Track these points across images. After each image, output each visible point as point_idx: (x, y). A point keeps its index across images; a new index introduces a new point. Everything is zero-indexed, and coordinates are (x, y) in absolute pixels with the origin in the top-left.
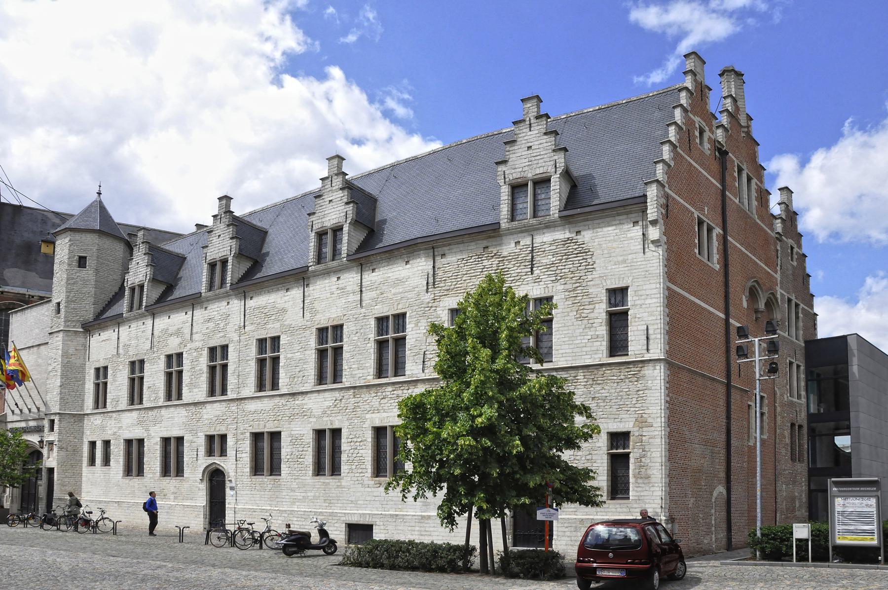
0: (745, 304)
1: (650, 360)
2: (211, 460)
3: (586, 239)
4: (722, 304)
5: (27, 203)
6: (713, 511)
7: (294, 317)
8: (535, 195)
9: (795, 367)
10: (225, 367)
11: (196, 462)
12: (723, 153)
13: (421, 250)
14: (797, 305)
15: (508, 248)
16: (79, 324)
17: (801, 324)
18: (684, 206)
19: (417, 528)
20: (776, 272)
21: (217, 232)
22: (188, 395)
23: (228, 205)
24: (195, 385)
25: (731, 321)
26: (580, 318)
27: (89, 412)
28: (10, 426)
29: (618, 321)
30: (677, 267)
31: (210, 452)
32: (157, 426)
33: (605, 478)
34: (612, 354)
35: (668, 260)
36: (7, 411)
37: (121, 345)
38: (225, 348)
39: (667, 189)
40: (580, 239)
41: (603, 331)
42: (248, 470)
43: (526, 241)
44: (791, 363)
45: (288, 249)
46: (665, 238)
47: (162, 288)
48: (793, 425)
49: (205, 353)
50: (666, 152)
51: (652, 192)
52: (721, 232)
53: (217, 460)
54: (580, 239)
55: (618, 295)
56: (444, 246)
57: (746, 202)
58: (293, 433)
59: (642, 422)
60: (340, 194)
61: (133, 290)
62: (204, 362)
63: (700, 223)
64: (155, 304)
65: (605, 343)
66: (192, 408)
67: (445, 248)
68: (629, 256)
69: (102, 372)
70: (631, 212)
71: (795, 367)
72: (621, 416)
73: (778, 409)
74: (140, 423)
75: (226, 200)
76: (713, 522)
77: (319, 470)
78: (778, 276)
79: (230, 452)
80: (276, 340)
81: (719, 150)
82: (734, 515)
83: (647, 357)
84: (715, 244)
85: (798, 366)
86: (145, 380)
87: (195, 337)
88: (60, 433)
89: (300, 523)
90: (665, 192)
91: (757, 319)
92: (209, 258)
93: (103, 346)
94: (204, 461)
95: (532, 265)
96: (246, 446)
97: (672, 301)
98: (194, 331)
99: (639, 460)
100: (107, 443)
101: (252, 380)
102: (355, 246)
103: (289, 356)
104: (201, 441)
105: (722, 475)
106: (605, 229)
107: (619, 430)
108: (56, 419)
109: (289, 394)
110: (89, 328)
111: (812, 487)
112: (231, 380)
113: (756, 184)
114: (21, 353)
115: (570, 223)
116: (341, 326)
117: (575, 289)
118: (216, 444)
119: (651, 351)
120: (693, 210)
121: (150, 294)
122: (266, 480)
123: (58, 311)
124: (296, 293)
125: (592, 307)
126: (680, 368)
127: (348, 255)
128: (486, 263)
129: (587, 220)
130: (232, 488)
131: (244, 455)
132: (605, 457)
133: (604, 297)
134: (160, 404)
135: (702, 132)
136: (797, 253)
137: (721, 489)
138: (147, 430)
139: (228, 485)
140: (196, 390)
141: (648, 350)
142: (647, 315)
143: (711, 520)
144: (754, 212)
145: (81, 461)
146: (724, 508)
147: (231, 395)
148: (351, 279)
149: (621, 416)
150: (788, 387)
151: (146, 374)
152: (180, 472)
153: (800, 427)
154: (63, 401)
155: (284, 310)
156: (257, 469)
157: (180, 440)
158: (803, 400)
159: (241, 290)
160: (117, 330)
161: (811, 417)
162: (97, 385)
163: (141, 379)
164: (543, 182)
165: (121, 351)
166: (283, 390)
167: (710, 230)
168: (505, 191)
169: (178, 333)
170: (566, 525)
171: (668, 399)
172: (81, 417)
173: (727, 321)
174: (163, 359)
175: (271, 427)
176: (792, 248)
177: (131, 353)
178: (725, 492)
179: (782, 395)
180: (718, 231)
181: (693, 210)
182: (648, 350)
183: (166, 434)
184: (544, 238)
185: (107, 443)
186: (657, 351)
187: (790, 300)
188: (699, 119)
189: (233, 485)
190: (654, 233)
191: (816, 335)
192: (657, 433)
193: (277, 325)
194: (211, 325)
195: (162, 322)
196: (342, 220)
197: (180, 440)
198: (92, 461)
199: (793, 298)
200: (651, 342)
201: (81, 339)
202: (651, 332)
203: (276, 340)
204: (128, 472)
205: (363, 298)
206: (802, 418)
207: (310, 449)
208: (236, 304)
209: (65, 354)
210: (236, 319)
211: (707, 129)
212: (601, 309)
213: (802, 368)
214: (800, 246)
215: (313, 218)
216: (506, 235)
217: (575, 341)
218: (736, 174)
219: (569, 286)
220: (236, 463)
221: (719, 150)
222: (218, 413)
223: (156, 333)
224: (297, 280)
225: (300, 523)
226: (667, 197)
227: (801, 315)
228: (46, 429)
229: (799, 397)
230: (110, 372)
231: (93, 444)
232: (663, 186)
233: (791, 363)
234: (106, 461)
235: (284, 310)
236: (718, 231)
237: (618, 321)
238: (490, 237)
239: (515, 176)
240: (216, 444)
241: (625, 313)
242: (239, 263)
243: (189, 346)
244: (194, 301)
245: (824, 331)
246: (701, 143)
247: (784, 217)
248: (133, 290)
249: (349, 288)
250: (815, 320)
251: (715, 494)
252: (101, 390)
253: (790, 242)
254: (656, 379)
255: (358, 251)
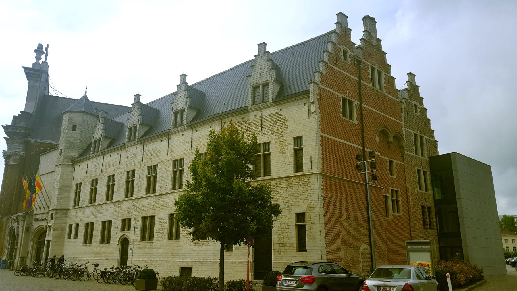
0: (377, 140)
1: (313, 174)
2: (123, 233)
3: (284, 113)
4: (360, 141)
5: (60, 95)
6: (360, 260)
7: (164, 155)
8: (263, 91)
9: (422, 173)
10: (133, 181)
11: (116, 235)
12: (359, 62)
13: (216, 120)
14: (421, 138)
15: (251, 117)
16: (70, 161)
17: (425, 148)
18: (333, 93)
19: (211, 269)
20: (401, 120)
21: (133, 113)
22: (116, 198)
23: (139, 99)
24: (119, 194)
25: (366, 149)
26: (282, 153)
27: (71, 208)
28: (34, 217)
29: (298, 153)
30: (327, 124)
31: (123, 229)
32: (97, 216)
33: (295, 239)
34: (296, 172)
35: (321, 121)
36: (34, 209)
37: (88, 171)
38: (134, 171)
39: (321, 86)
40: (282, 112)
41: (292, 159)
42: (139, 238)
43: (259, 114)
44: (419, 171)
45: (168, 120)
46: (319, 111)
47: (109, 141)
48: (423, 207)
49: (125, 174)
50: (321, 67)
51: (312, 87)
52: (359, 103)
53: (126, 233)
54: (282, 112)
55: (298, 140)
56: (225, 118)
57: (377, 85)
58: (160, 216)
59: (310, 207)
60: (184, 93)
61: (130, 129)
62: (124, 178)
63: (344, 100)
64: (106, 148)
65: (292, 165)
66: (117, 204)
67: (226, 119)
68: (302, 121)
69: (79, 186)
70: (303, 98)
71: (422, 173)
72: (301, 204)
73: (411, 198)
74: (93, 213)
75: (138, 96)
76: (361, 266)
77: (170, 238)
78: (403, 123)
79: (132, 228)
80: (156, 166)
81: (357, 60)
82: (41, 213)
83: (312, 172)
84: (355, 110)
85: (425, 173)
86: (97, 190)
87: (121, 166)
88: (55, 221)
89: (160, 268)
90: (319, 87)
91: (389, 147)
92: (129, 125)
93: (83, 172)
94: (120, 234)
95: (262, 126)
96: (139, 225)
97: (324, 142)
98: (121, 163)
99: (310, 228)
100: (77, 225)
101: (144, 188)
102: (191, 118)
103: (161, 175)
104: (120, 223)
105: (366, 238)
106: (292, 107)
107: (300, 212)
108: (54, 212)
109: (160, 195)
110: (74, 163)
111: (441, 245)
112: (136, 188)
113: (385, 75)
114: (42, 177)
115: (277, 105)
116: (183, 159)
117: (279, 138)
118: (126, 224)
119: (313, 169)
120: (338, 94)
121: (140, 132)
122: (146, 243)
123: (61, 154)
124: (165, 142)
125: (287, 147)
126: (330, 177)
127: (186, 123)
128: (243, 126)
129: (285, 103)
130: (131, 249)
131: (138, 230)
132: (295, 227)
133: (292, 141)
134: (103, 202)
135: (345, 53)
136: (420, 108)
137: (365, 246)
138: (96, 217)
139: (130, 247)
140: (119, 195)
141: (311, 168)
142: (311, 150)
143: (359, 265)
144: (384, 90)
145: (64, 236)
146: (369, 257)
147: (135, 196)
148: (188, 134)
149: (301, 204)
150: (418, 184)
151: (98, 186)
152: (109, 241)
153: (429, 208)
154: (59, 202)
155: (160, 151)
156: (143, 238)
157: (110, 222)
158: (430, 192)
159: (142, 142)
160: (120, 154)
161: (436, 201)
162: (76, 193)
163: (96, 189)
164: (266, 85)
165: (88, 174)
166: (157, 193)
167: (351, 103)
168: (251, 90)
169: (114, 164)
170: (278, 267)
171: (323, 194)
172: (67, 210)
173: (364, 150)
174: (106, 178)
175: (151, 214)
176: (416, 106)
177: (92, 176)
178: (369, 248)
179: (413, 189)
180: (356, 103)
181: (338, 94)
182: (311, 168)
183: (104, 220)
184: (267, 112)
185: (77, 225)
186: (316, 169)
187: (415, 135)
188: (343, 46)
189: (132, 247)
190: (313, 108)
191: (438, 153)
192: (317, 213)
193: (157, 159)
194: (129, 160)
195: (151, 146)
196: (185, 106)
197: (110, 222)
198: (70, 237)
199: (418, 133)
200: (313, 164)
201: (70, 168)
202: (312, 159)
203: (156, 166)
204: (85, 242)
205: (193, 145)
206: (430, 203)
207: (167, 225)
208: (140, 148)
209: (62, 177)
210: (139, 157)
211: (349, 51)
212: (291, 148)
213: (428, 173)
214: (422, 104)
215: (173, 105)
216: (251, 112)
217: (281, 164)
218: (370, 72)
219: (277, 137)
220: (134, 235)
221: (357, 60)
222: (129, 207)
223: (104, 164)
224: (166, 136)
225: (160, 268)
226: (320, 89)
227: (425, 143)
228: (49, 219)
229: (427, 190)
230: (82, 186)
231: (71, 226)
232: (318, 84)
233: (419, 171)
234: (76, 236)
235: (160, 151)
236: (356, 103)
237: (298, 153)
238: (244, 113)
239: (255, 83)
240: (126, 224)
241: (302, 149)
242: (142, 128)
243: (118, 171)
244: (168, 134)
245: (442, 151)
246: (345, 58)
247: (409, 89)
248: (95, 142)
249: (187, 140)
250: (436, 144)
251: (361, 249)
252: (78, 195)
253: (414, 102)
254: (316, 183)
255: (192, 121)
